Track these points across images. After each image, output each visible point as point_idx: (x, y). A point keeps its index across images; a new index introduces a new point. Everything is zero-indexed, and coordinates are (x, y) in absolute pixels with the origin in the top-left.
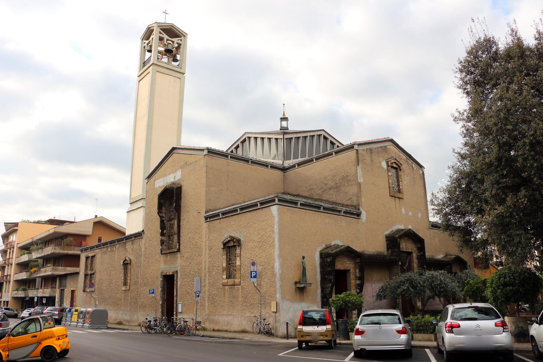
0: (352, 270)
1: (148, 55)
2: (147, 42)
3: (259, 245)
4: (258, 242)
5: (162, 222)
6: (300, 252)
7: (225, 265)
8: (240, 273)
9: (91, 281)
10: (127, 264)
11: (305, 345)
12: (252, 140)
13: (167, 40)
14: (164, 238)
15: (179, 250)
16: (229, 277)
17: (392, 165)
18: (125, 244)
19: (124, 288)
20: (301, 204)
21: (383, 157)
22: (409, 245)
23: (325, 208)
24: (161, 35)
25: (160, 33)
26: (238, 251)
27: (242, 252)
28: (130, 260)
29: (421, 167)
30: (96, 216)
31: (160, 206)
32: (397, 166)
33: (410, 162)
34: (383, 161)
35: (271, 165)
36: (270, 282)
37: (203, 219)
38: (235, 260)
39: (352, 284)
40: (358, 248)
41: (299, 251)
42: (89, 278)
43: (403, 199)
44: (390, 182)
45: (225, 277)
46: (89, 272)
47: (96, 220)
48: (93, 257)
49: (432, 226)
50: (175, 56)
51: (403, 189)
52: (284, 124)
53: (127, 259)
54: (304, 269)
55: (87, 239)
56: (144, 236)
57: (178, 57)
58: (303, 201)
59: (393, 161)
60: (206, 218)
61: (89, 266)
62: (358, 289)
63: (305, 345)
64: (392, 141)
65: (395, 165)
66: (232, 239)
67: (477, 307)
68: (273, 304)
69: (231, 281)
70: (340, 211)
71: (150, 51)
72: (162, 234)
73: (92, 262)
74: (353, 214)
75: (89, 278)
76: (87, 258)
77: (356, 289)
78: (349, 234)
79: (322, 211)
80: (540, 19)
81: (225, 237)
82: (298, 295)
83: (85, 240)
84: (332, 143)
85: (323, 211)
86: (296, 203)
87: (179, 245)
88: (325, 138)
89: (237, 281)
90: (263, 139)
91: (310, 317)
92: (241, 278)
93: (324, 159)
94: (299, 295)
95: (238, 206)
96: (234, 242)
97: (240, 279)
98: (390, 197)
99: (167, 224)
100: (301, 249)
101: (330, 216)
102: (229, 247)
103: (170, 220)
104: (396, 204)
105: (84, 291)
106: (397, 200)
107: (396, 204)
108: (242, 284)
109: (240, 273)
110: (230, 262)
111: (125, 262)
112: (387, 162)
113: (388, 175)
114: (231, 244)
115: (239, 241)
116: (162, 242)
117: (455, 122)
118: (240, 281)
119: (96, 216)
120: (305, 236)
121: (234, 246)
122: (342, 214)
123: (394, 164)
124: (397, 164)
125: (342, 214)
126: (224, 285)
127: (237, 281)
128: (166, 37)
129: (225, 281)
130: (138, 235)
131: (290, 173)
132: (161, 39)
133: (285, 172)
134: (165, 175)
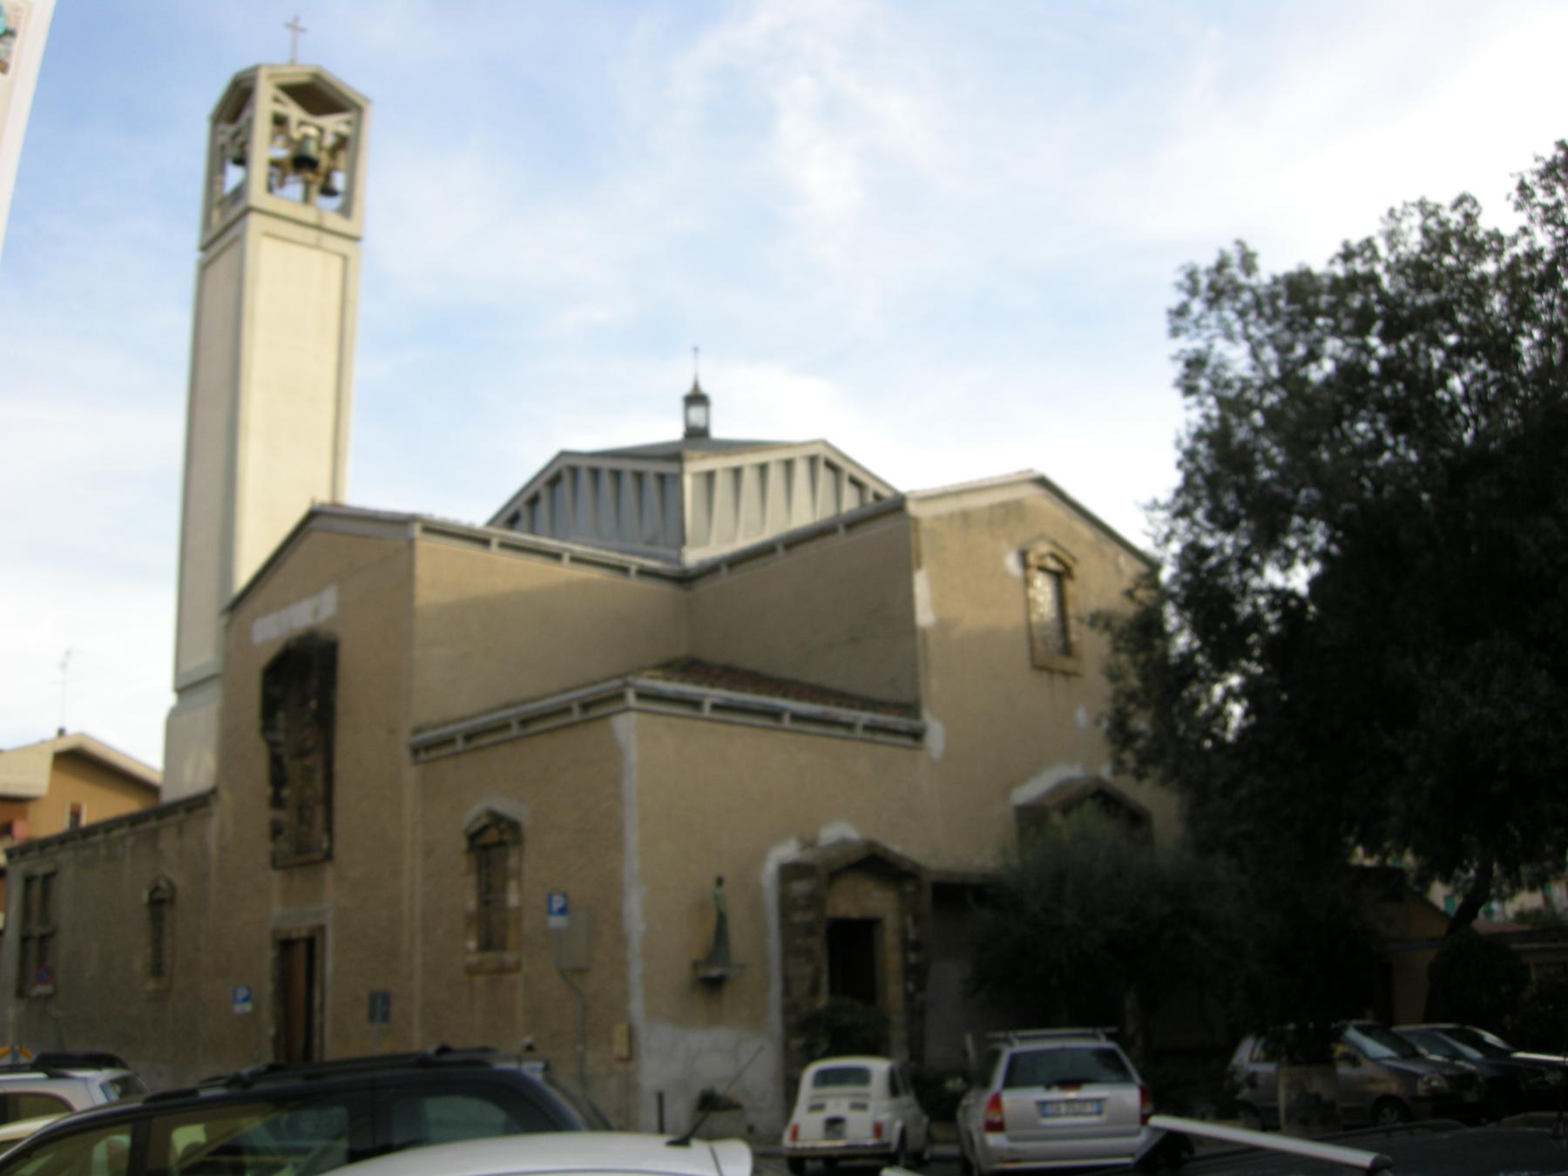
0: (891, 922)
1: (234, 175)
2: (231, 129)
5: (276, 761)
7: (471, 904)
9: (42, 959)
10: (161, 902)
12: (585, 479)
13: (302, 123)
14: (282, 816)
15: (329, 856)
16: (487, 945)
18: (154, 834)
19: (151, 985)
20: (715, 707)
23: (796, 717)
24: (280, 109)
25: (276, 100)
26: (513, 862)
28: (172, 888)
30: (61, 732)
31: (270, 707)
33: (1111, 549)
37: (406, 755)
38: (504, 889)
40: (904, 845)
42: (33, 947)
45: (472, 944)
46: (37, 930)
47: (64, 745)
48: (48, 877)
50: (328, 176)
52: (697, 415)
53: (163, 884)
54: (722, 919)
55: (32, 809)
56: (216, 808)
57: (339, 181)
60: (415, 751)
61: (35, 907)
64: (1043, 482)
66: (496, 819)
68: (620, 1032)
69: (491, 958)
70: (849, 726)
71: (241, 161)
72: (277, 802)
73: (46, 894)
74: (895, 732)
75: (33, 947)
76: (28, 880)
80: (1181, 277)
81: (474, 812)
83: (24, 815)
84: (855, 482)
86: (696, 704)
87: (331, 839)
88: (830, 465)
89: (510, 958)
90: (617, 475)
95: (511, 712)
96: (501, 832)
99: (293, 767)
102: (486, 847)
103: (302, 753)
105: (21, 993)
106: (1059, 681)
110: (490, 894)
111: (158, 895)
112: (1023, 556)
114: (491, 836)
115: (514, 827)
116: (276, 831)
119: (61, 732)
121: (501, 844)
126: (472, 971)
127: (510, 958)
128: (294, 112)
129: (474, 959)
130: (197, 804)
131: (703, 587)
132: (280, 121)
134: (285, 604)
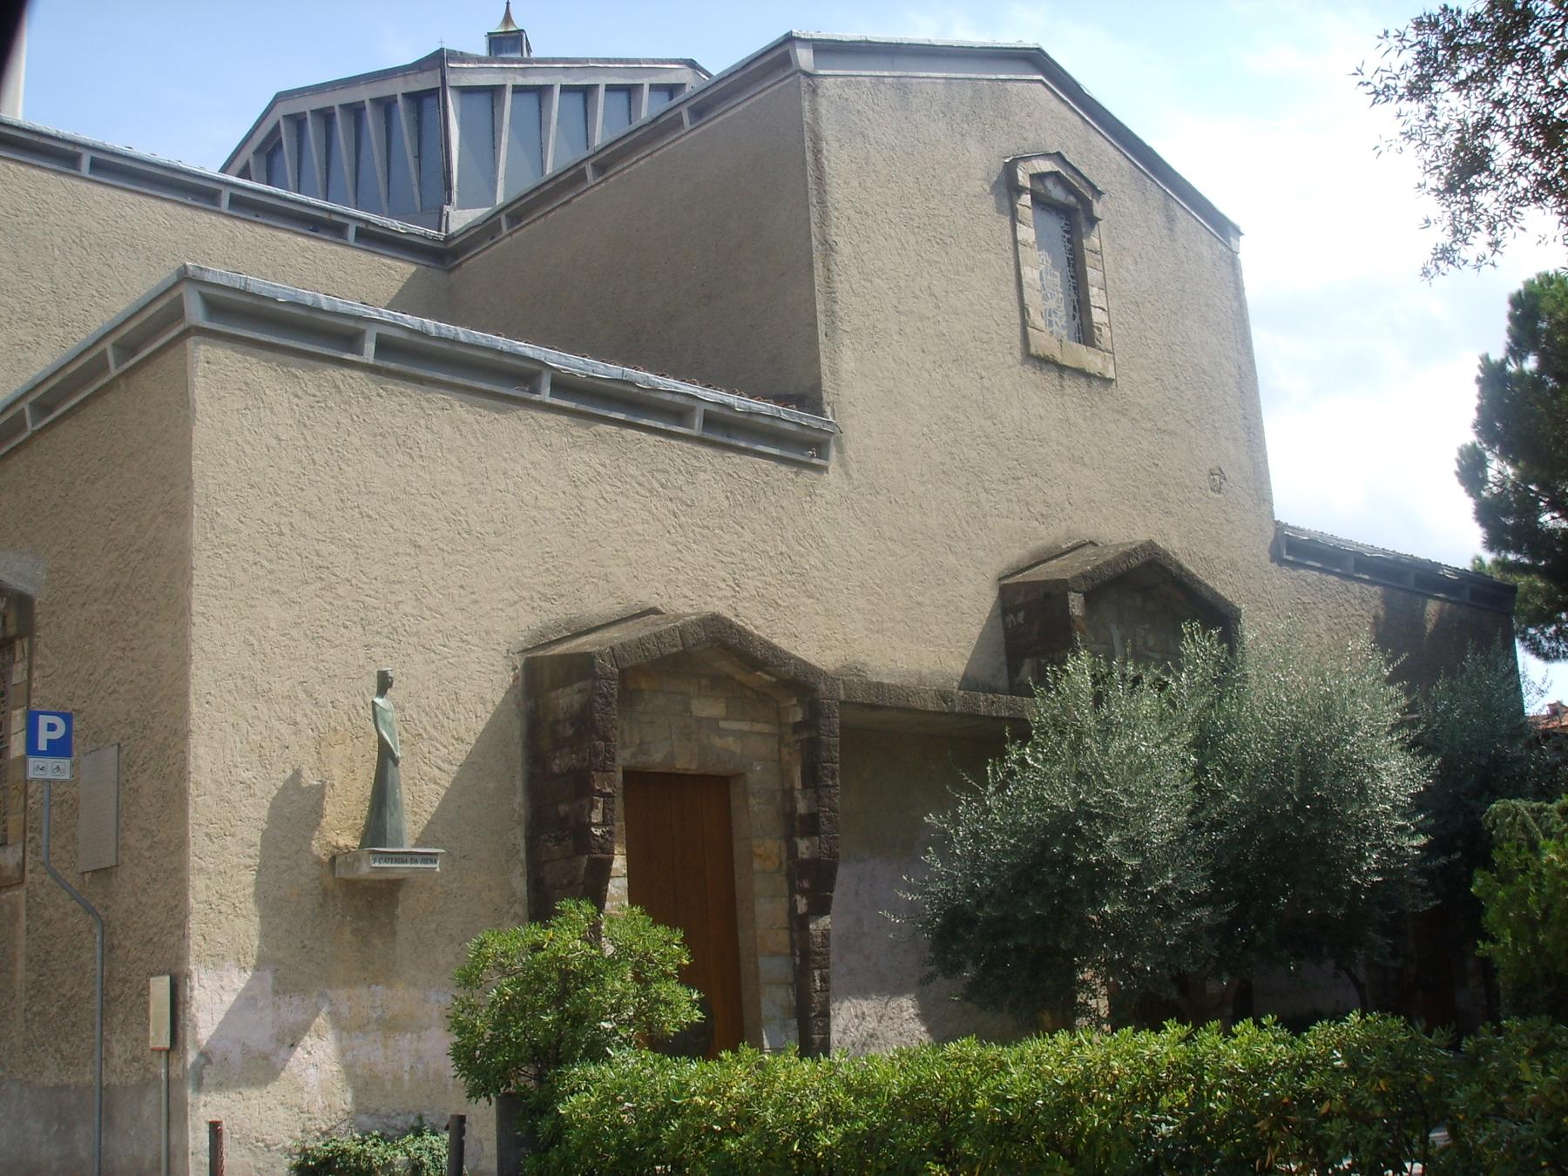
3: (107, 611)
4: (106, 592)
8: (25, 806)
17: (1039, 188)
22: (1151, 642)
23: (564, 385)
27: (36, 674)
29: (1222, 227)
32: (1072, 199)
35: (362, 225)
36: (150, 847)
39: (756, 865)
41: (369, 639)
44: (1024, 280)
59: (1046, 166)
62: (803, 892)
65: (1058, 193)
77: (793, 890)
78: (746, 555)
79: (549, 400)
82: (348, 936)
85: (556, 401)
91: (184, 1105)
92: (29, 835)
93: (635, 159)
94: (355, 932)
97: (20, 845)
101: (304, 250)
108: (29, 876)
109: (25, 806)
117: (1407, 140)
118: (24, 858)
120: (411, 550)
123: (1049, 184)
124: (1069, 189)
131: (475, 262)
133: (450, 271)
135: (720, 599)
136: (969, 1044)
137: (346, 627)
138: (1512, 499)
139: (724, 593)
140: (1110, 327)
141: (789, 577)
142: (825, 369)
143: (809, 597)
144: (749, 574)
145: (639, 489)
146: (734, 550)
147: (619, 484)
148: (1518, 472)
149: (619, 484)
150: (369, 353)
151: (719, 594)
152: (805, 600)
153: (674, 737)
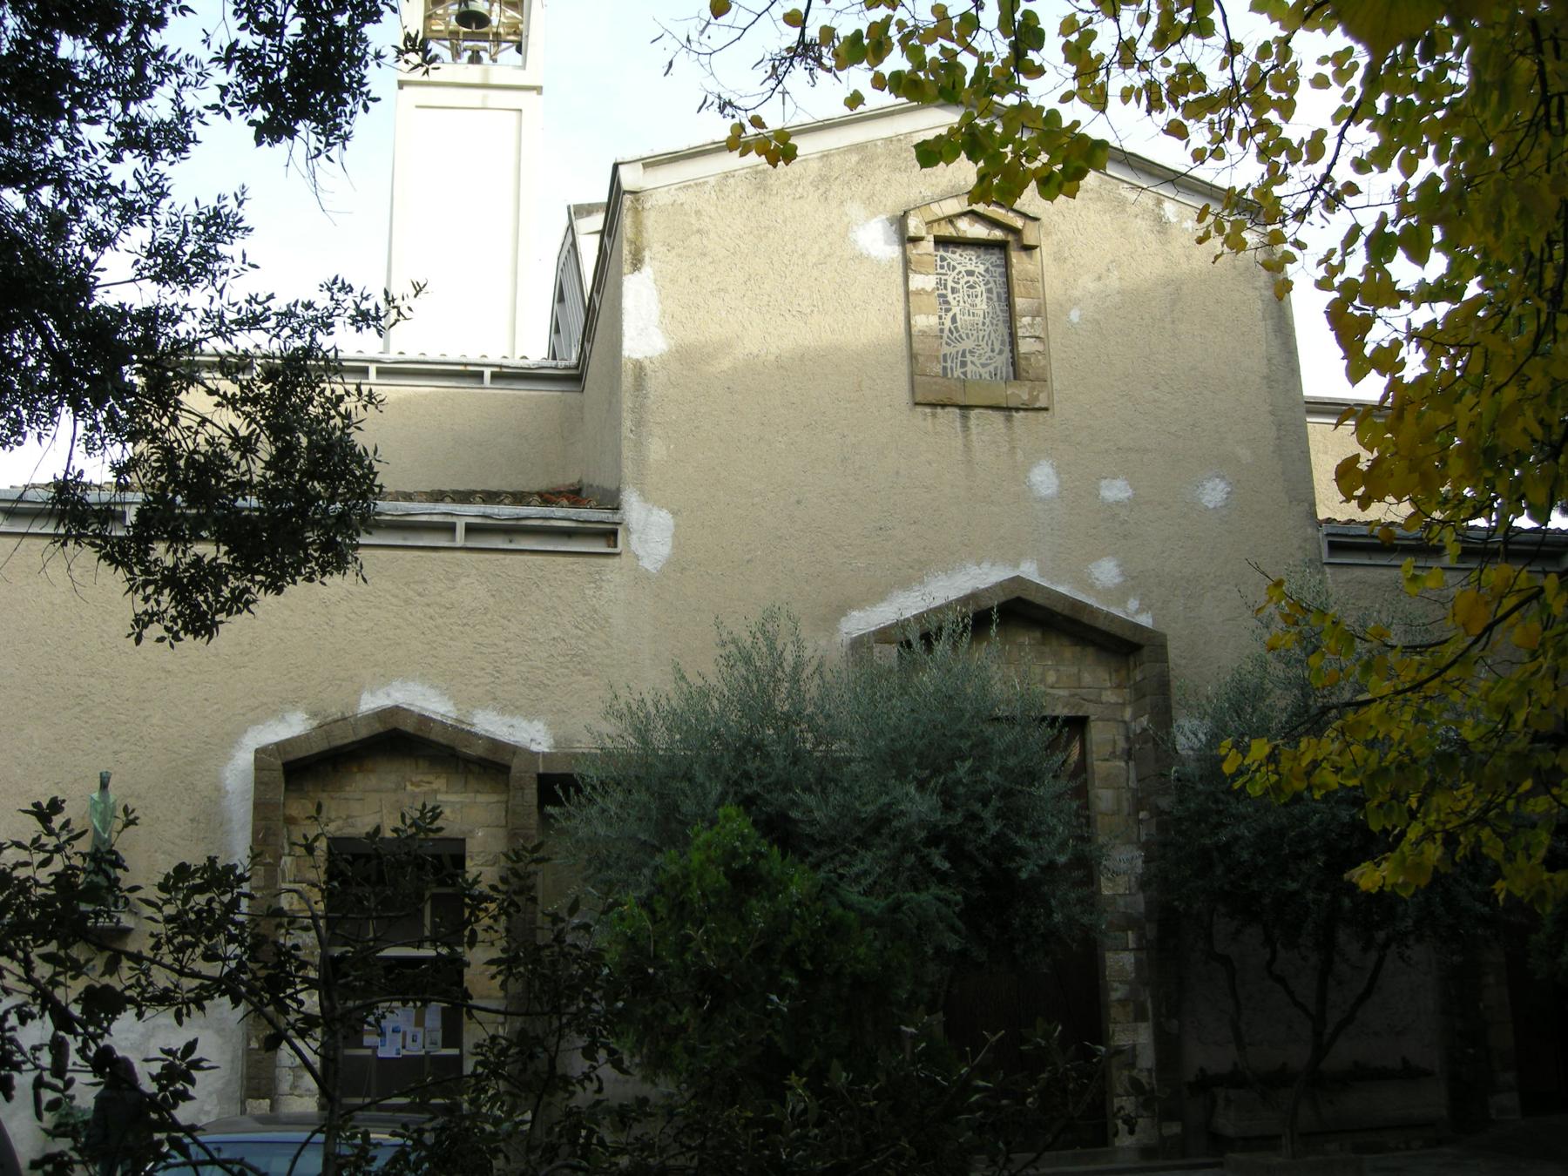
6: (115, 753)
11: (1465, 492)
20: (471, 529)
21: (869, 201)
34: (867, 219)
41: (116, 747)
43: (1046, 409)
49: (1335, 547)
51: (1045, 354)
58: (472, 512)
63: (1465, 492)
67: (925, 141)
78: (509, 645)
86: (450, 529)
98: (919, 409)
100: (126, 741)
104: (968, 447)
107: (968, 447)
113: (907, 293)
120: (163, 675)
122: (460, 539)
125: (460, 539)
135: (476, 686)
136: (526, 1099)
137: (98, 739)
138: (961, 1140)
139: (482, 680)
140: (1516, 151)
141: (561, 659)
142: (627, 452)
143: (584, 675)
144: (514, 660)
145: (394, 600)
146: (496, 641)
147: (372, 598)
148: (1359, 891)
149: (372, 598)
150: (487, 372)
151: (476, 682)
152: (581, 677)
153: (385, 811)
